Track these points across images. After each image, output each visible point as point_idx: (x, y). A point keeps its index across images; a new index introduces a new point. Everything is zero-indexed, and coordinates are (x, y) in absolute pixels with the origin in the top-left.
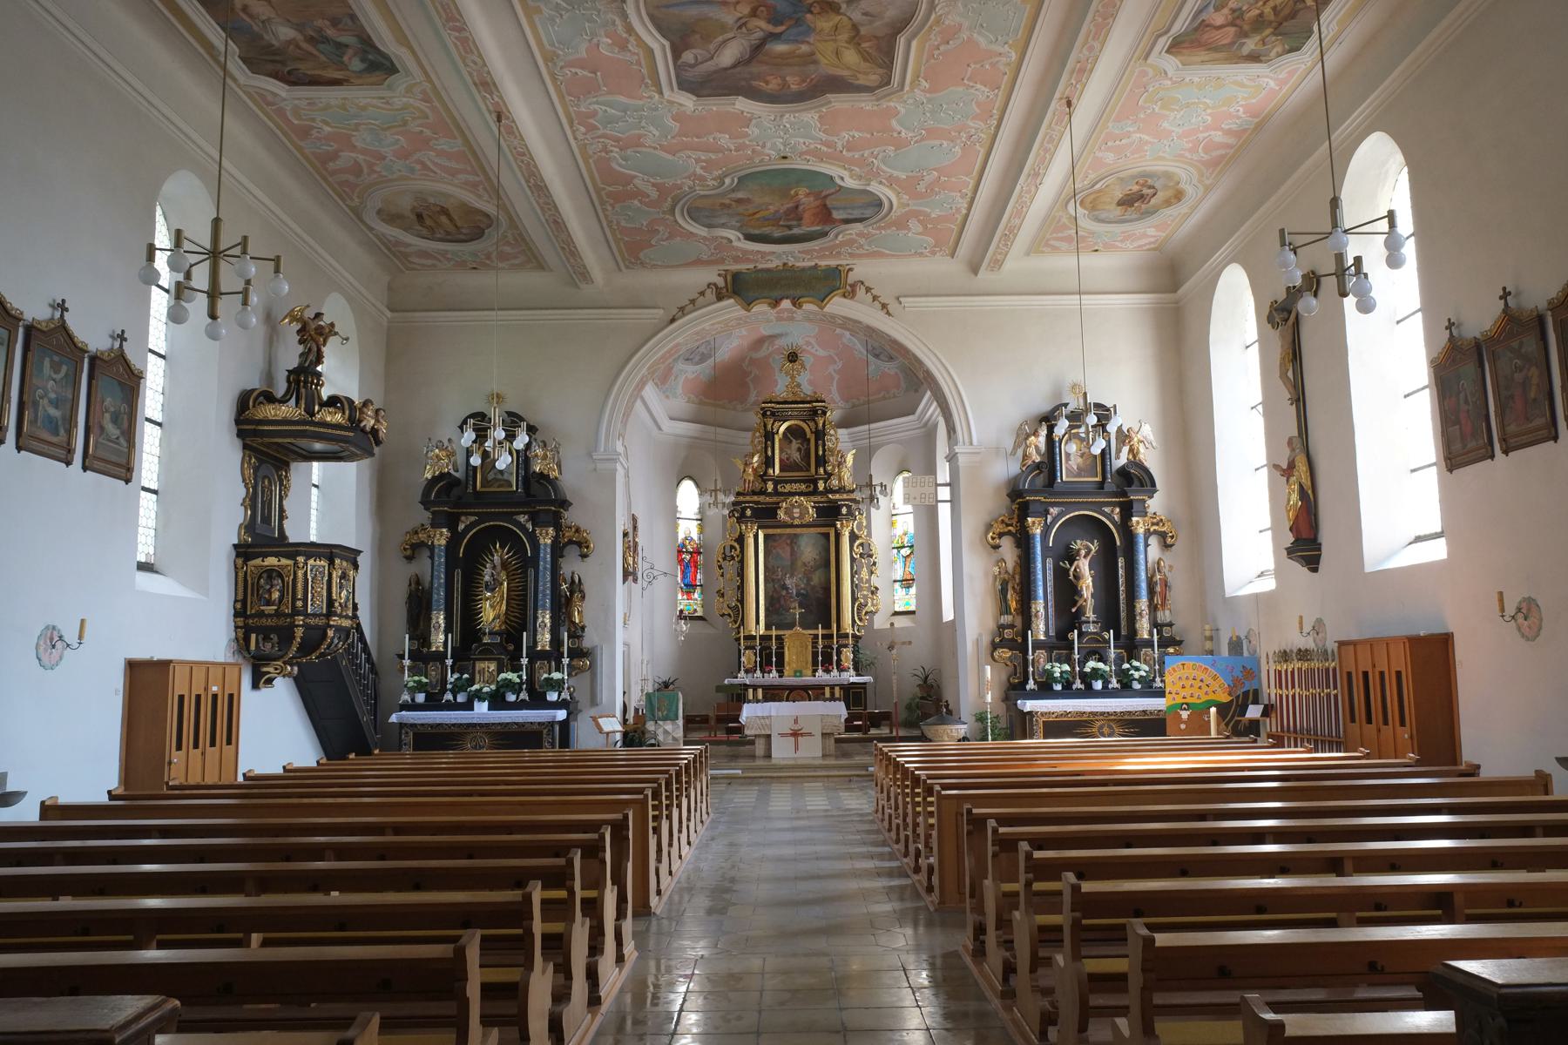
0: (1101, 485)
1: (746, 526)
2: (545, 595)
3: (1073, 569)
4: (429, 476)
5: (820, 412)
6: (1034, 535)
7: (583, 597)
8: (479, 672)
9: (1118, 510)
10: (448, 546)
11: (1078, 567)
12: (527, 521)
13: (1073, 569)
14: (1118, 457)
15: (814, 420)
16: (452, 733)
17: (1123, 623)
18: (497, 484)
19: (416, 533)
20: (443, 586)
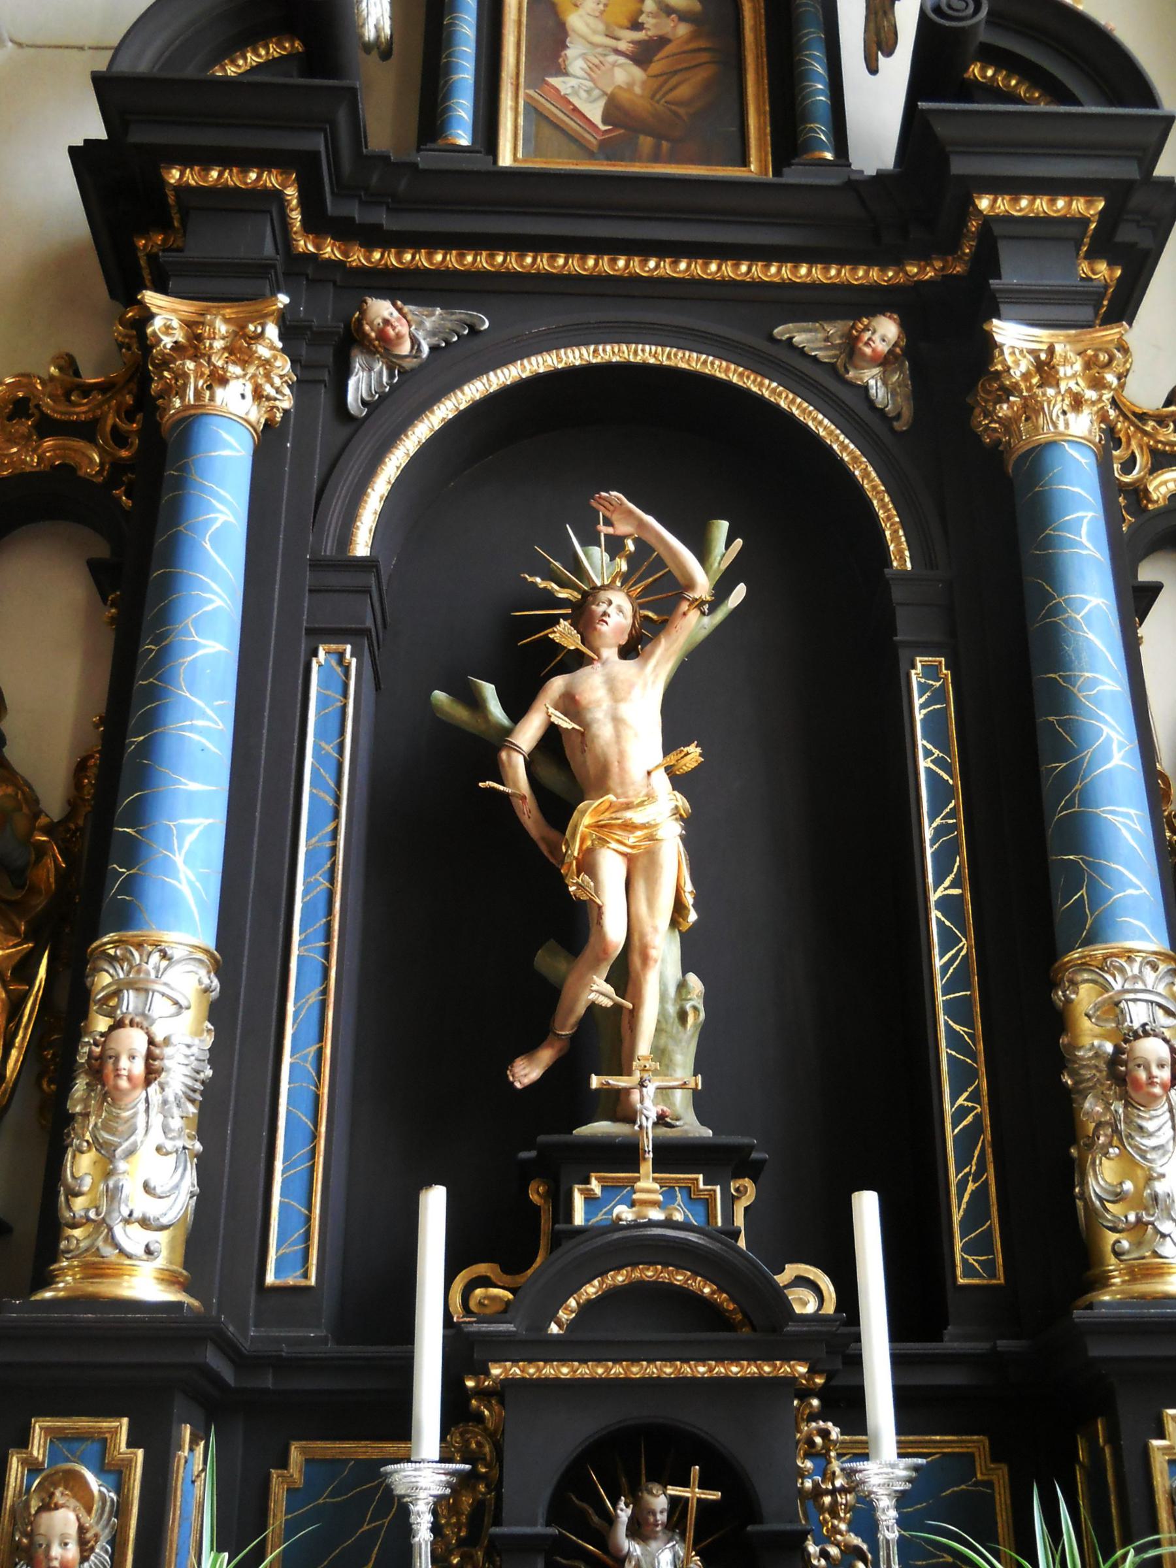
13: (528, 734)
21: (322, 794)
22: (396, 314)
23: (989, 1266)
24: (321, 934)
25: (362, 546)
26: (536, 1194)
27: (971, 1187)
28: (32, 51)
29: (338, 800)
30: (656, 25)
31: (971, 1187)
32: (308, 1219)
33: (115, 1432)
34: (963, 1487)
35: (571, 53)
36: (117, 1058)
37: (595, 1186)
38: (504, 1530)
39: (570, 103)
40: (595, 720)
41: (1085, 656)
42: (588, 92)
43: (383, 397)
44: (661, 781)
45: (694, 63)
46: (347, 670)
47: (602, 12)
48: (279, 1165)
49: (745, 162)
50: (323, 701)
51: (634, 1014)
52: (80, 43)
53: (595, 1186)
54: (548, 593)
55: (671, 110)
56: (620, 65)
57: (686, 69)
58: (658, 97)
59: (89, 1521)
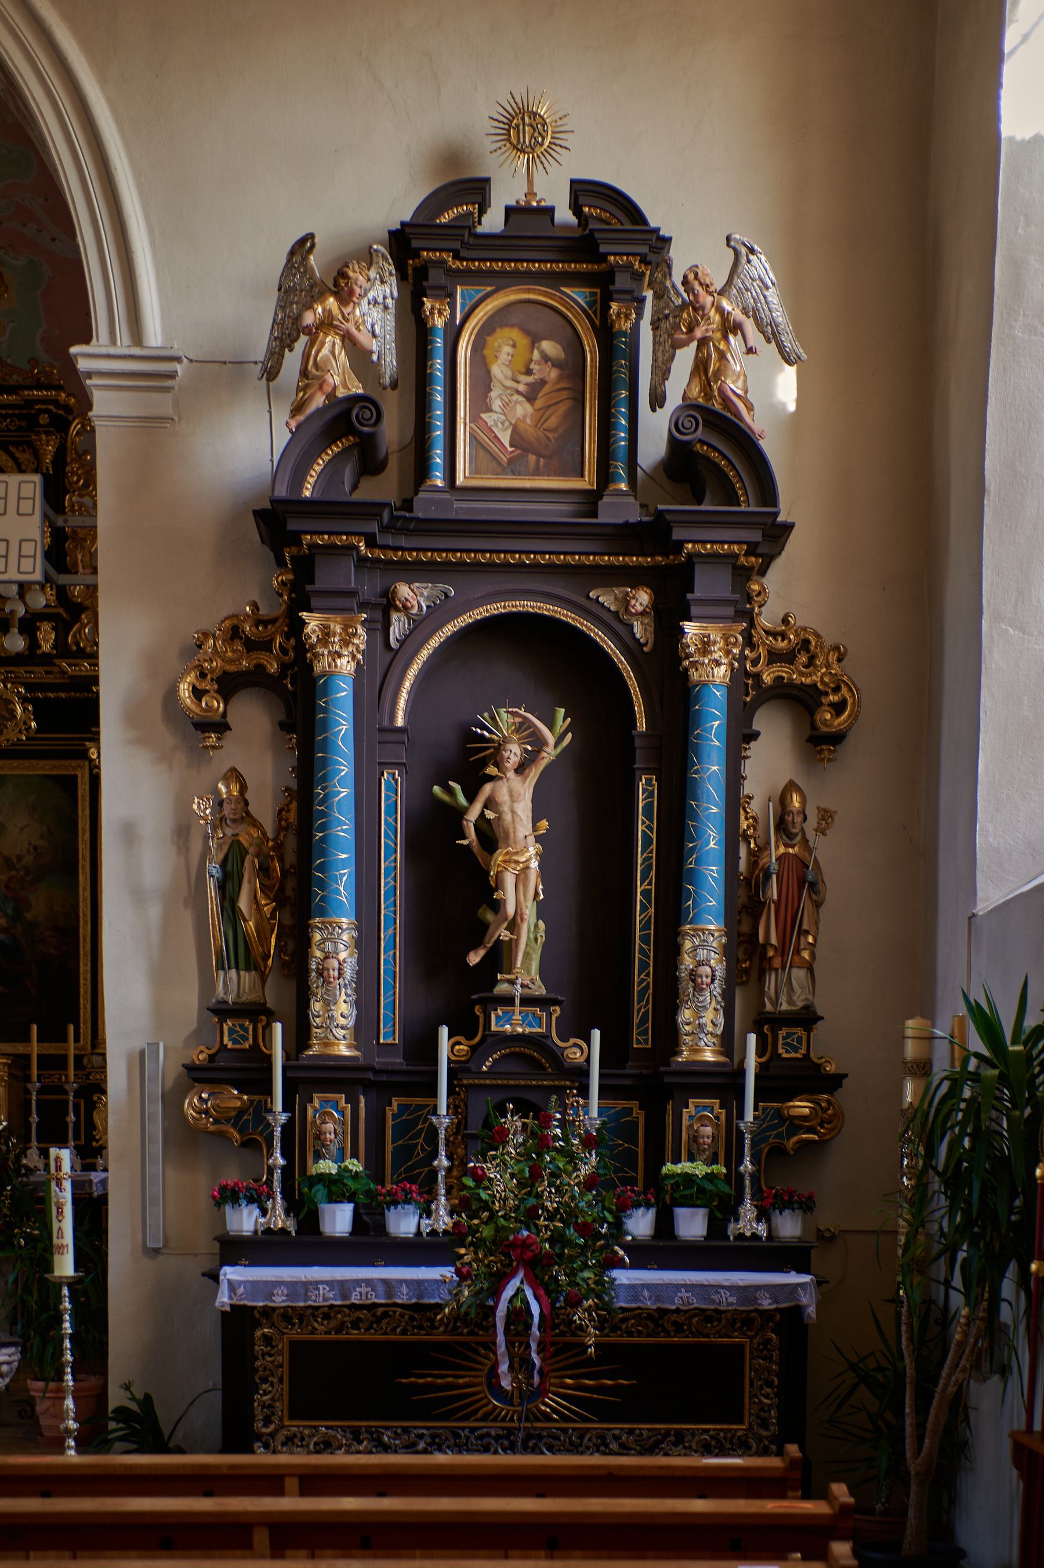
0: (590, 500)
3: (473, 815)
5: (44, 419)
6: (329, 675)
9: (643, 598)
11: (490, 803)
13: (473, 815)
14: (657, 400)
15: (30, 445)
17: (642, 1008)
21: (390, 842)
22: (411, 594)
23: (646, 1041)
24: (393, 905)
25: (400, 722)
26: (478, 1010)
27: (643, 1010)
28: (198, 364)
29: (396, 844)
30: (539, 371)
31: (643, 1010)
32: (394, 1019)
33: (340, 1099)
34: (400, 1142)
35: (493, 394)
36: (328, 970)
37: (500, 1012)
38: (469, 1132)
39: (493, 432)
40: (504, 811)
41: (705, 796)
42: (502, 423)
43: (407, 637)
44: (531, 839)
45: (559, 399)
46: (396, 781)
47: (510, 361)
48: (382, 998)
49: (582, 475)
50: (387, 797)
51: (517, 940)
52: (224, 360)
53: (500, 1012)
54: (483, 735)
55: (545, 435)
56: (520, 403)
57: (556, 403)
58: (539, 426)
59: (336, 1127)
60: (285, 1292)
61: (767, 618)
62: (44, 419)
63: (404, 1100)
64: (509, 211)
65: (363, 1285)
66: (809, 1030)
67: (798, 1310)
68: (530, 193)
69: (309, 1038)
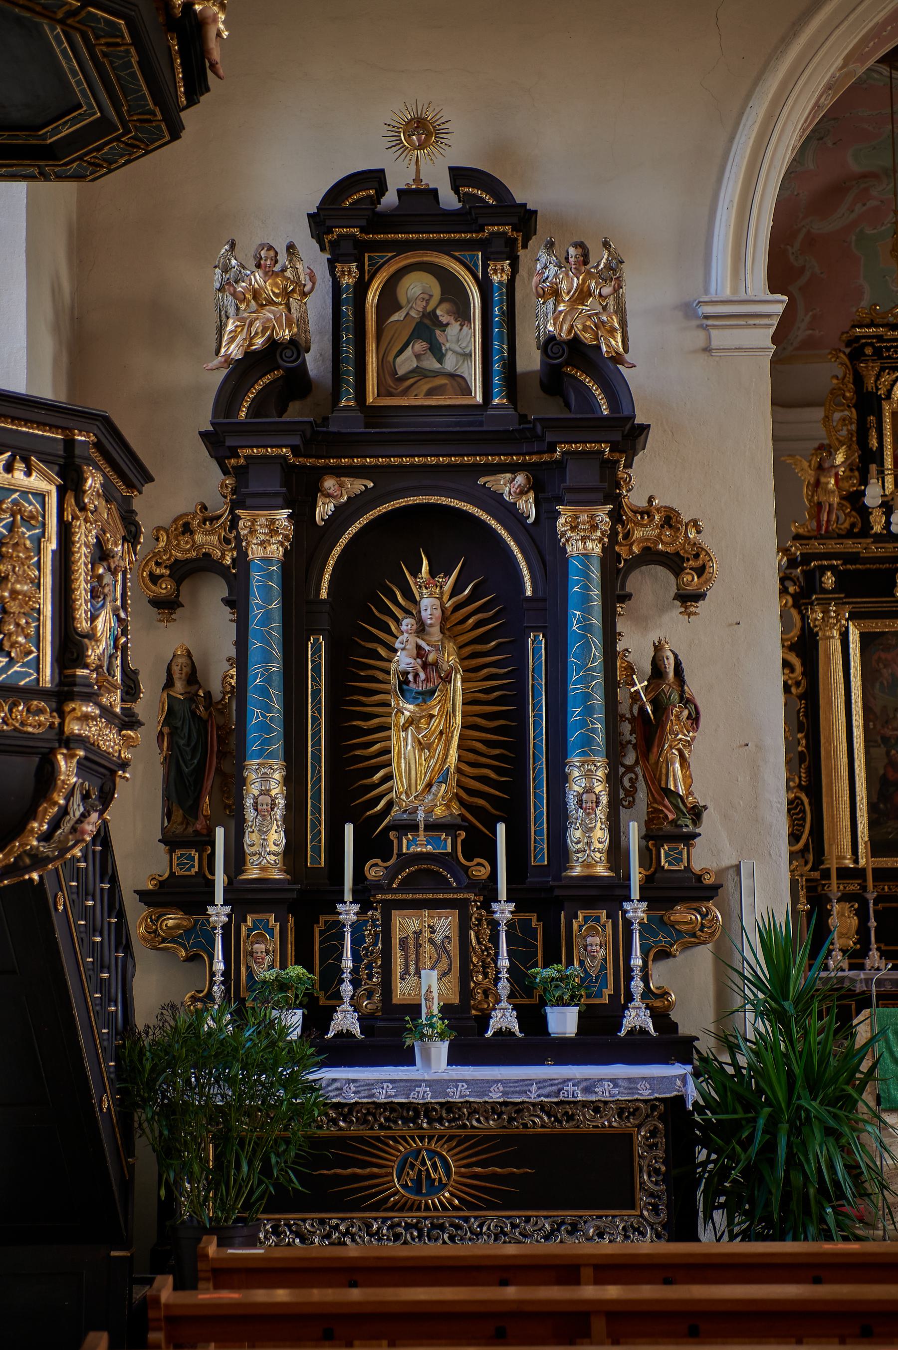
1: (826, 612)
2: (589, 711)
4: (234, 350)
5: (869, 351)
7: (695, 719)
8: (403, 942)
10: (286, 564)
12: (522, 493)
16: (341, 1142)
18: (425, 386)
19: (187, 529)
20: (278, 680)
60: (501, 1089)
61: (635, 498)
62: (869, 351)
63: (256, 916)
64: (400, 192)
65: (571, 1084)
66: (689, 846)
67: (680, 1100)
68: (418, 180)
69: (244, 863)
